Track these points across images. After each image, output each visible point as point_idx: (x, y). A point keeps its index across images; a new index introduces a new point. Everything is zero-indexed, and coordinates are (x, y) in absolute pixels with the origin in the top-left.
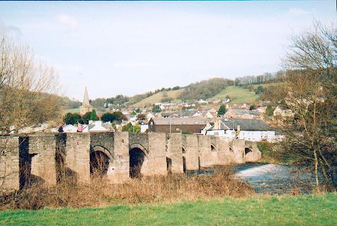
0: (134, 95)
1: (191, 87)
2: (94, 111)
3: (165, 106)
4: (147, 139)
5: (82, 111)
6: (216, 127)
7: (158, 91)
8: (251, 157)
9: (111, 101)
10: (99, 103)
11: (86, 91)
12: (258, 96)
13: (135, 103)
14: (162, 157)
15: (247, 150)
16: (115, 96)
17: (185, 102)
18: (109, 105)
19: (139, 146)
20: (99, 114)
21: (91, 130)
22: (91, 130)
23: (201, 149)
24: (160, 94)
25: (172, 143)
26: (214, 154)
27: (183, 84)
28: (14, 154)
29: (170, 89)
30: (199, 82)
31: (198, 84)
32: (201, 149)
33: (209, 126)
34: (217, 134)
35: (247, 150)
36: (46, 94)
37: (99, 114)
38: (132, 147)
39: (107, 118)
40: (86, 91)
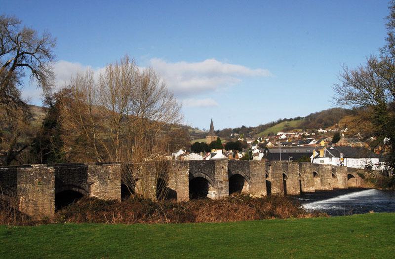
0: (258, 125)
1: (311, 117)
3: (286, 135)
4: (249, 167)
5: (209, 140)
6: (321, 155)
7: (280, 122)
8: (354, 183)
9: (236, 131)
10: (227, 132)
11: (212, 122)
12: (63, 125)
13: (259, 133)
15: (350, 176)
16: (240, 127)
17: (306, 131)
18: (235, 134)
20: (224, 142)
21: (213, 158)
22: (213, 158)
23: (304, 176)
24: (282, 125)
25: (273, 170)
30: (319, 112)
31: (317, 114)
32: (304, 176)
33: (315, 154)
35: (350, 176)
36: (181, 125)
37: (224, 142)
39: (228, 147)
40: (212, 122)
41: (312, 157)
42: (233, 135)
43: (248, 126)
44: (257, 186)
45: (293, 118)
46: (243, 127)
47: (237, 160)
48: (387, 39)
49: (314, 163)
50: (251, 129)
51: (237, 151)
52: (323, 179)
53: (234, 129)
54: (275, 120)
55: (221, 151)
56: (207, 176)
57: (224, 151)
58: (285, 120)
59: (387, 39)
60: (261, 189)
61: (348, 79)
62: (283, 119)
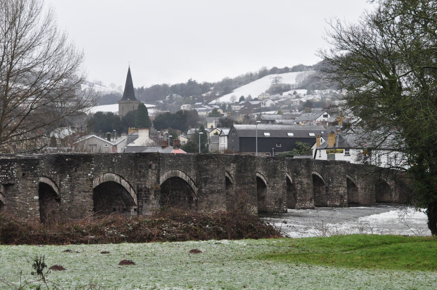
7: (263, 73)
9: (177, 89)
29: (286, 70)
41: (314, 148)
42: (171, 97)
43: (200, 81)
44: (210, 198)
45: (290, 66)
46: (192, 84)
47: (221, 124)
48: (250, 96)
49: (317, 158)
50: (206, 87)
51: (178, 131)
52: (330, 188)
53: (172, 86)
54: (255, 69)
55: (148, 131)
56: (123, 181)
57: (153, 130)
58: (275, 71)
59: (250, 96)
60: (217, 203)
61: (340, 38)
62: (269, 68)
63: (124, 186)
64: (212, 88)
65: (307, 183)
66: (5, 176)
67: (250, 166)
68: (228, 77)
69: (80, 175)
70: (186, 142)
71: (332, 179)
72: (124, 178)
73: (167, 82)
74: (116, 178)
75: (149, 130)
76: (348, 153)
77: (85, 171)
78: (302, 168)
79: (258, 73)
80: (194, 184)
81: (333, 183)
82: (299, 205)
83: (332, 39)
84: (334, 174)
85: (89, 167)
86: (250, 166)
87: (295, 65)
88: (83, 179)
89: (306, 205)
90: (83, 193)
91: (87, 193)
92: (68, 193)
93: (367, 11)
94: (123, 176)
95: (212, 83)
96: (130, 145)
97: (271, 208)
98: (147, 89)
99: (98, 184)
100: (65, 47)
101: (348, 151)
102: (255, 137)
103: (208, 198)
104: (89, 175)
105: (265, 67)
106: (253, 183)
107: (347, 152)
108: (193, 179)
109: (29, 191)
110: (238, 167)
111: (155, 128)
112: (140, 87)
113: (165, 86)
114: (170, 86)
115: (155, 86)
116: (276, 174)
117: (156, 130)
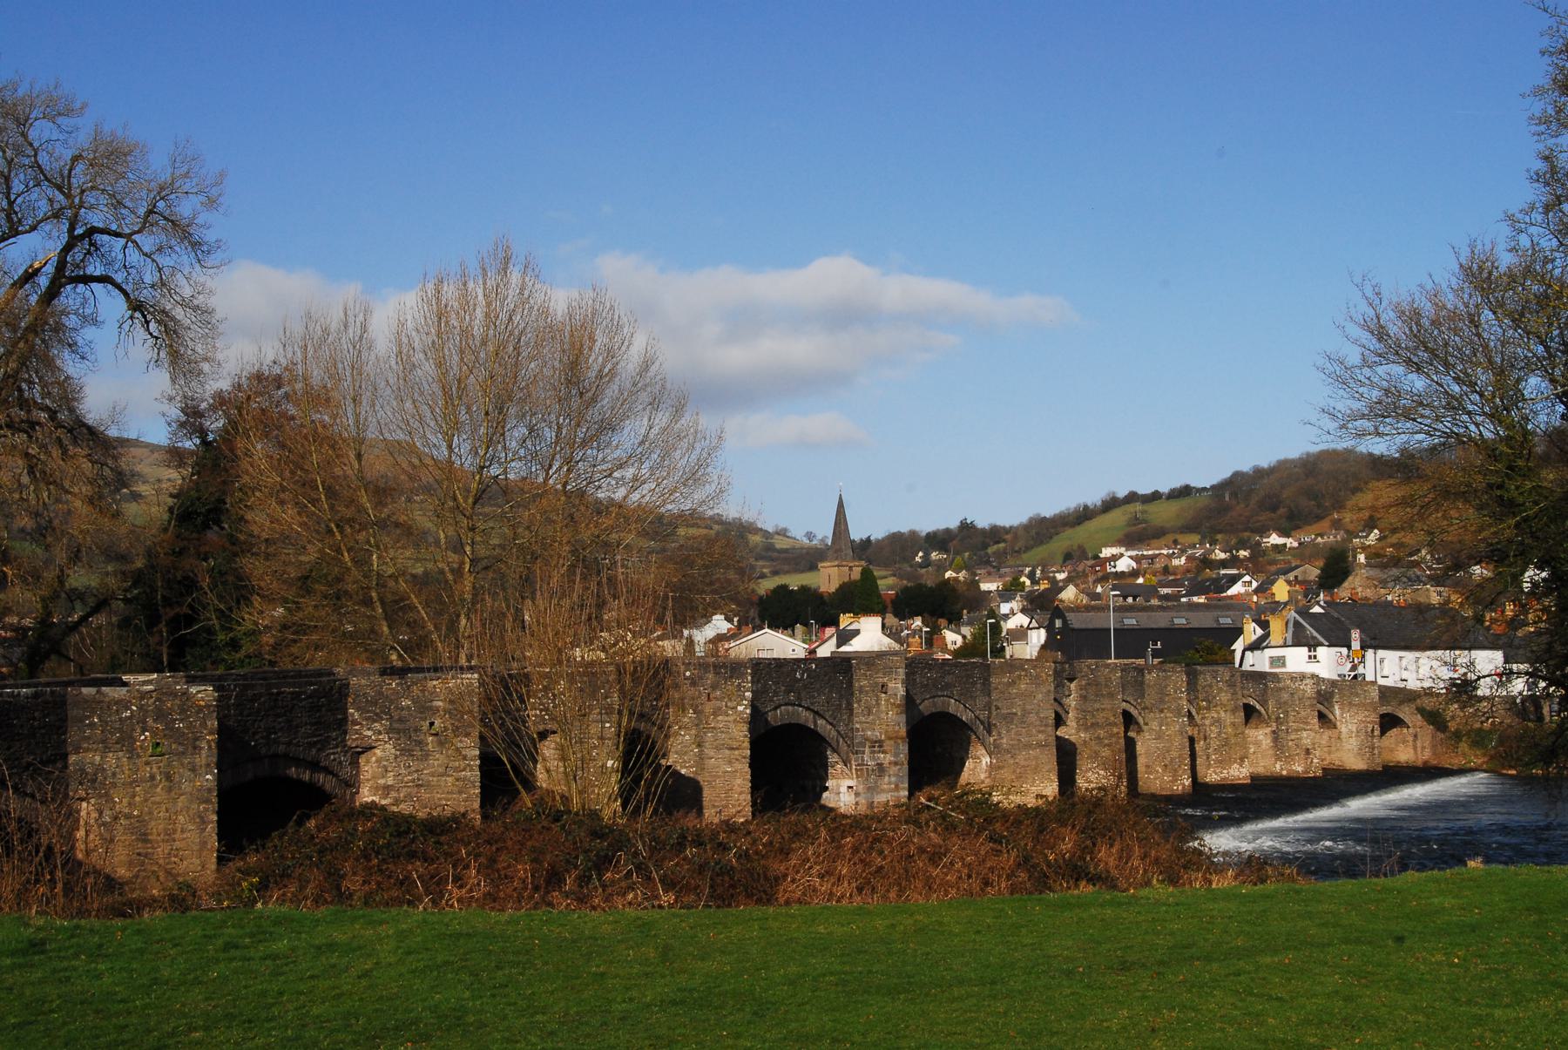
1: (1235, 486)
2: (866, 573)
5: (828, 579)
6: (1277, 635)
7: (1111, 504)
8: (1404, 749)
9: (939, 540)
10: (901, 546)
11: (841, 505)
14: (1039, 745)
15: (1389, 722)
19: (953, 707)
20: (888, 584)
25: (1084, 698)
26: (1260, 736)
27: (1207, 474)
28: (1052, 781)
29: (1156, 496)
31: (1259, 473)
33: (1252, 631)
34: (1280, 661)
35: (1389, 722)
37: (888, 584)
38: (926, 707)
40: (841, 505)
41: (1238, 646)
42: (926, 557)
43: (982, 523)
45: (1164, 489)
46: (966, 527)
49: (1246, 667)
50: (996, 534)
51: (942, 622)
52: (1282, 735)
53: (928, 535)
54: (1094, 498)
56: (820, 722)
57: (891, 620)
60: (1036, 770)
63: (823, 734)
64: (1008, 537)
65: (1233, 724)
66: (538, 712)
67: (1106, 686)
68: (1039, 515)
69: (720, 708)
70: (958, 645)
71: (1286, 713)
72: (823, 717)
73: (917, 528)
74: (805, 717)
75: (883, 619)
76: (1315, 657)
77: (730, 700)
78: (1220, 690)
79: (1099, 503)
80: (984, 727)
81: (1287, 722)
82: (1214, 772)
83: (1356, 332)
84: (1290, 703)
85: (740, 690)
86: (1106, 686)
87: (1173, 487)
88: (726, 718)
89: (1232, 772)
90: (727, 752)
91: (736, 752)
92: (692, 751)
93: (1456, 250)
94: (822, 712)
95: (1007, 526)
96: (844, 649)
97: (1155, 779)
98: (878, 541)
99: (763, 731)
100: (651, 373)
101: (1315, 651)
102: (1105, 626)
103: (1017, 761)
104: (740, 708)
105: (1114, 493)
106: (1115, 724)
107: (1312, 654)
108: (981, 717)
109: (595, 747)
110: (1081, 689)
111: (896, 616)
112: (864, 537)
113: (913, 534)
114: (924, 534)
115: (894, 534)
116: (1165, 703)
117: (896, 620)
